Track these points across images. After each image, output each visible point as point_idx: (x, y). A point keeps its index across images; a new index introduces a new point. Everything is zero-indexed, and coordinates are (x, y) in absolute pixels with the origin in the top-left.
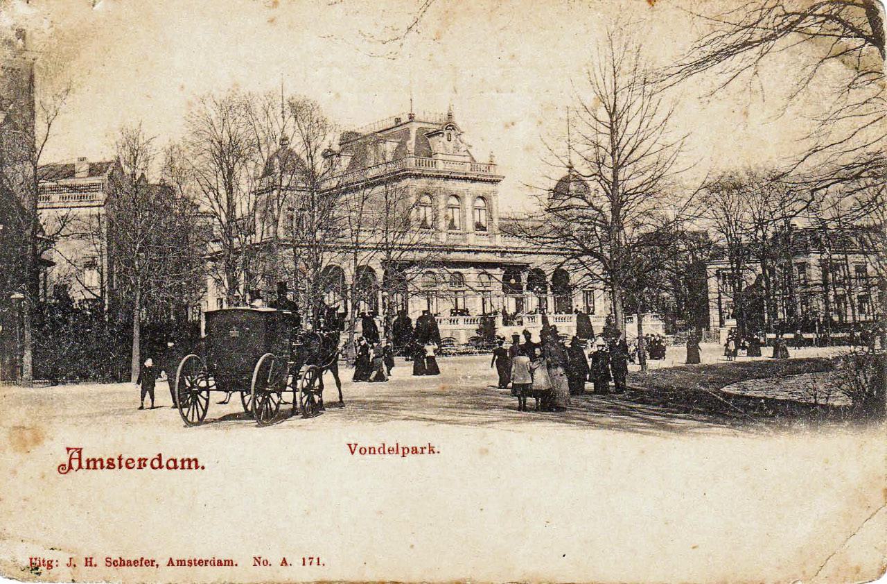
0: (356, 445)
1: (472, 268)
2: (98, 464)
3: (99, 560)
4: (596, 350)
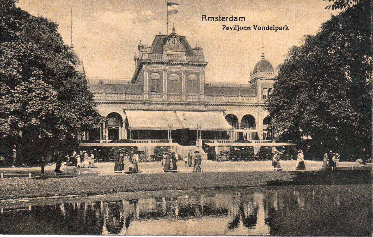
0: (257, 26)
1: (304, 43)
2: (212, 19)
3: (252, 29)
4: (282, 133)
